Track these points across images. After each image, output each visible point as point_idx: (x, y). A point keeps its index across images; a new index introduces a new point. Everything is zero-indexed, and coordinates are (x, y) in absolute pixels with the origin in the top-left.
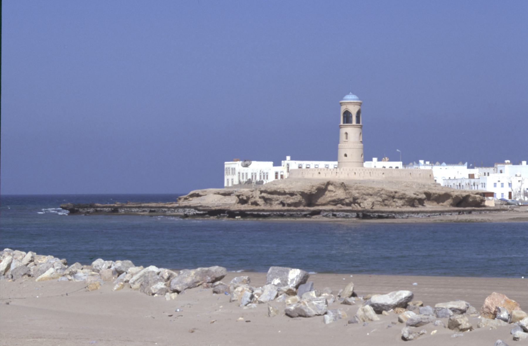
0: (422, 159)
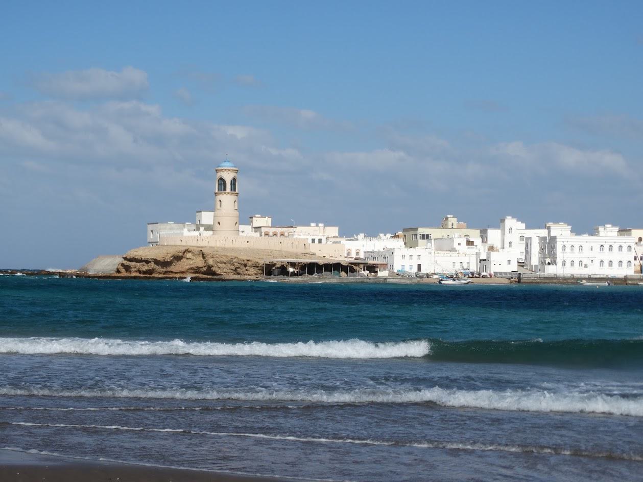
0: (313, 222)
